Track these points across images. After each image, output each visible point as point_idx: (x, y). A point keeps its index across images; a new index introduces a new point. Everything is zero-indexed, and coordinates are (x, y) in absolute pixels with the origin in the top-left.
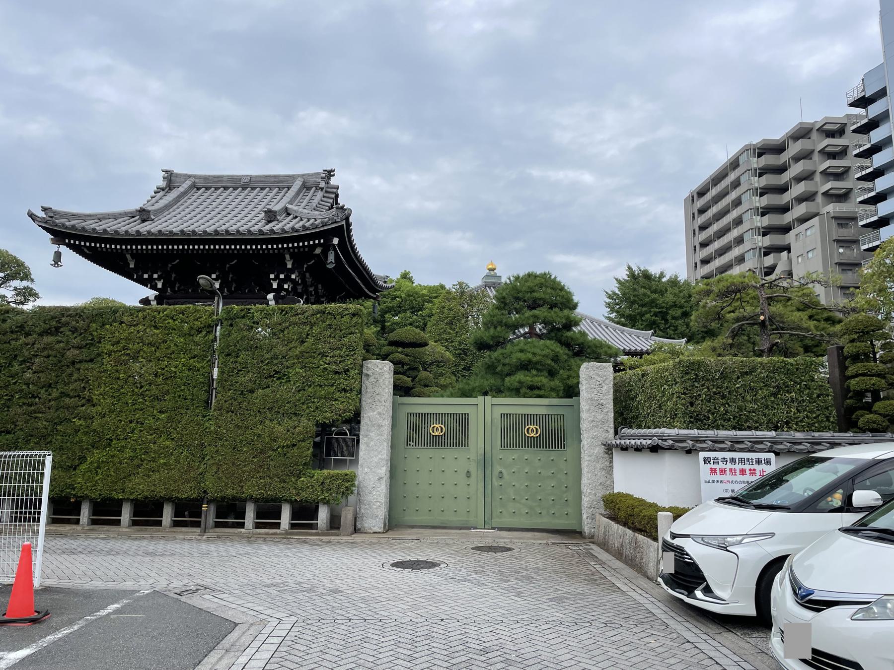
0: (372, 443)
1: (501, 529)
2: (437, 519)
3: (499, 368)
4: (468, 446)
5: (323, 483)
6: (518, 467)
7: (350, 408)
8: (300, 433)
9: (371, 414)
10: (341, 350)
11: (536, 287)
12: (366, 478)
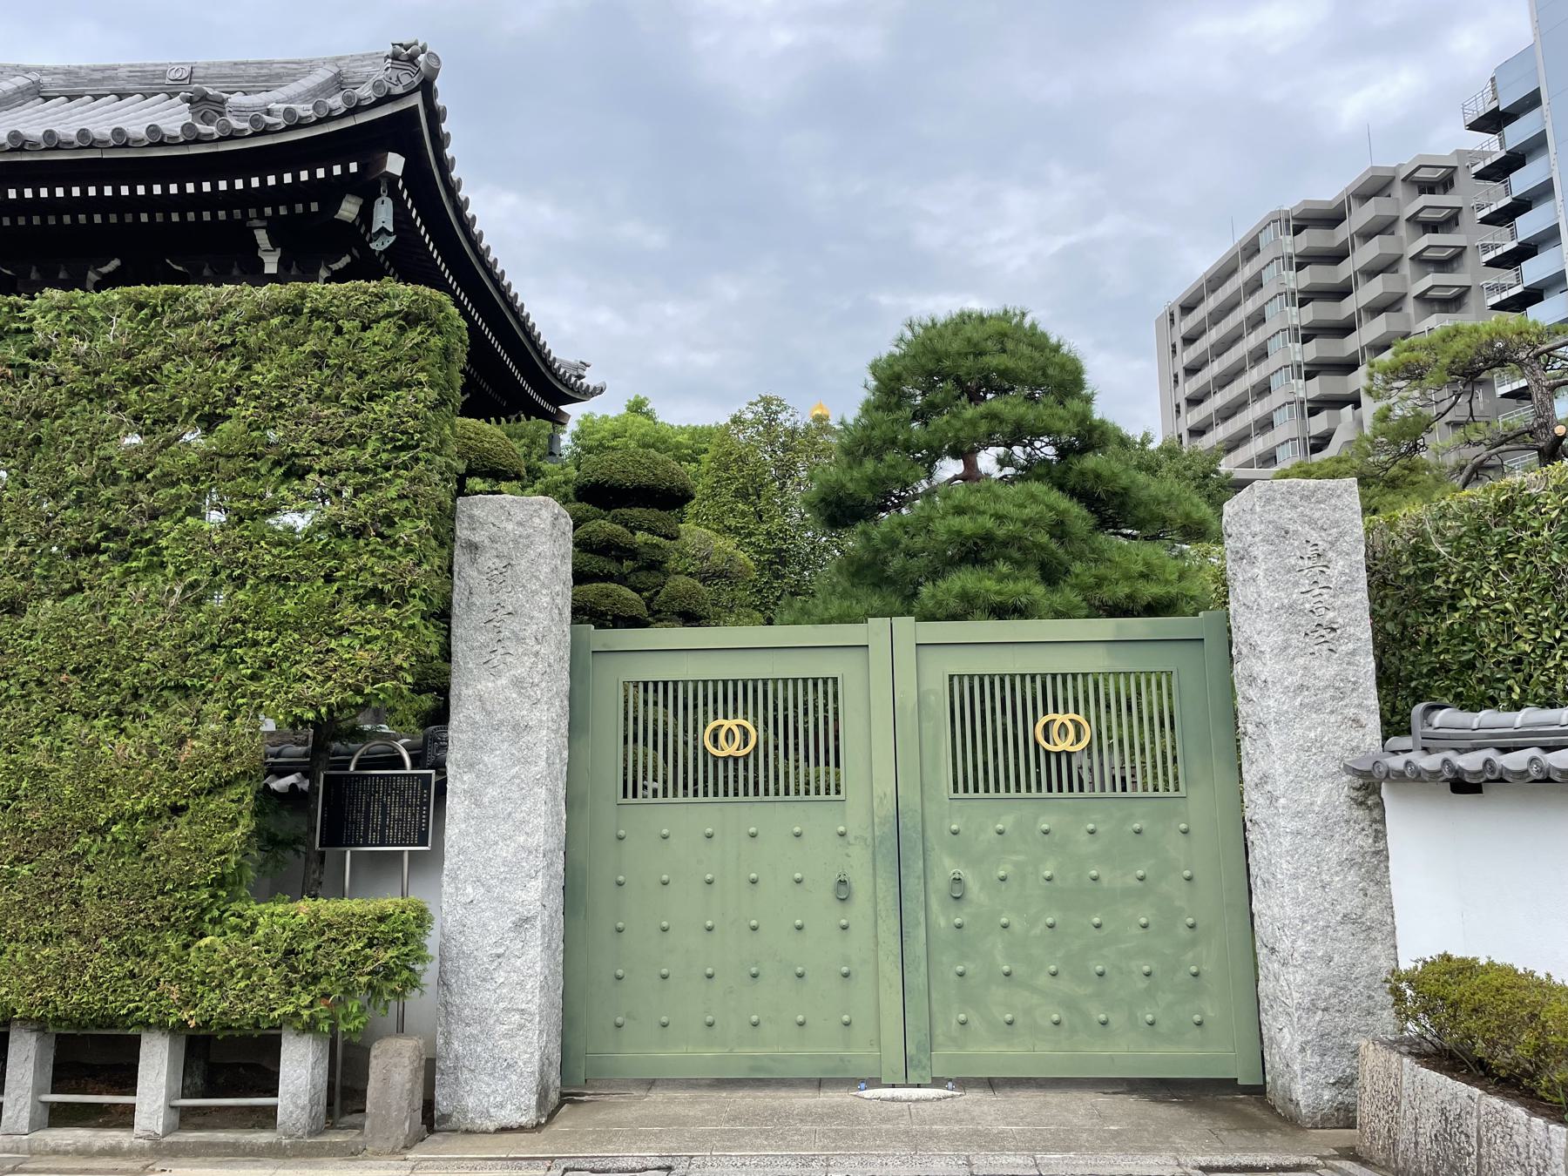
0: (492, 792)
1: (963, 1083)
2: (743, 1055)
3: (896, 563)
4: (838, 792)
5: (290, 952)
6: (1021, 858)
7: (398, 661)
8: (201, 762)
9: (486, 685)
10: (362, 446)
11: (989, 343)
12: (472, 920)
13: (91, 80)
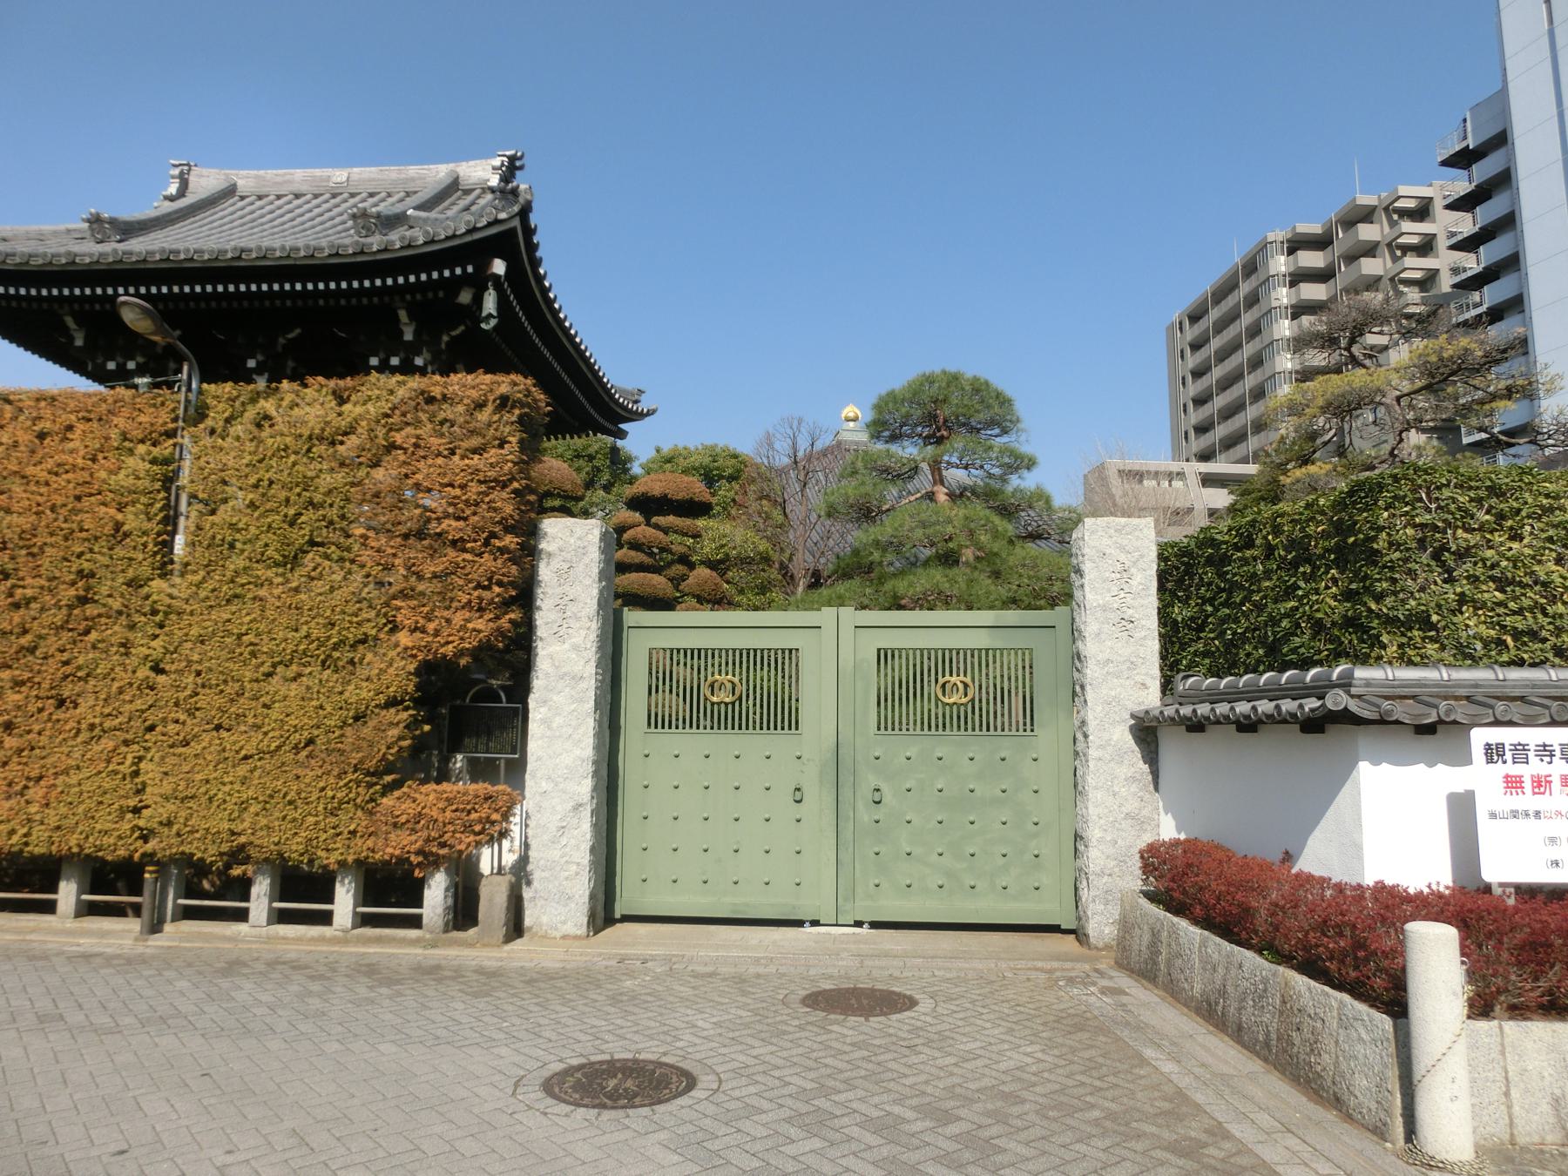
0: (558, 721)
4: (797, 729)
13: (276, 183)
